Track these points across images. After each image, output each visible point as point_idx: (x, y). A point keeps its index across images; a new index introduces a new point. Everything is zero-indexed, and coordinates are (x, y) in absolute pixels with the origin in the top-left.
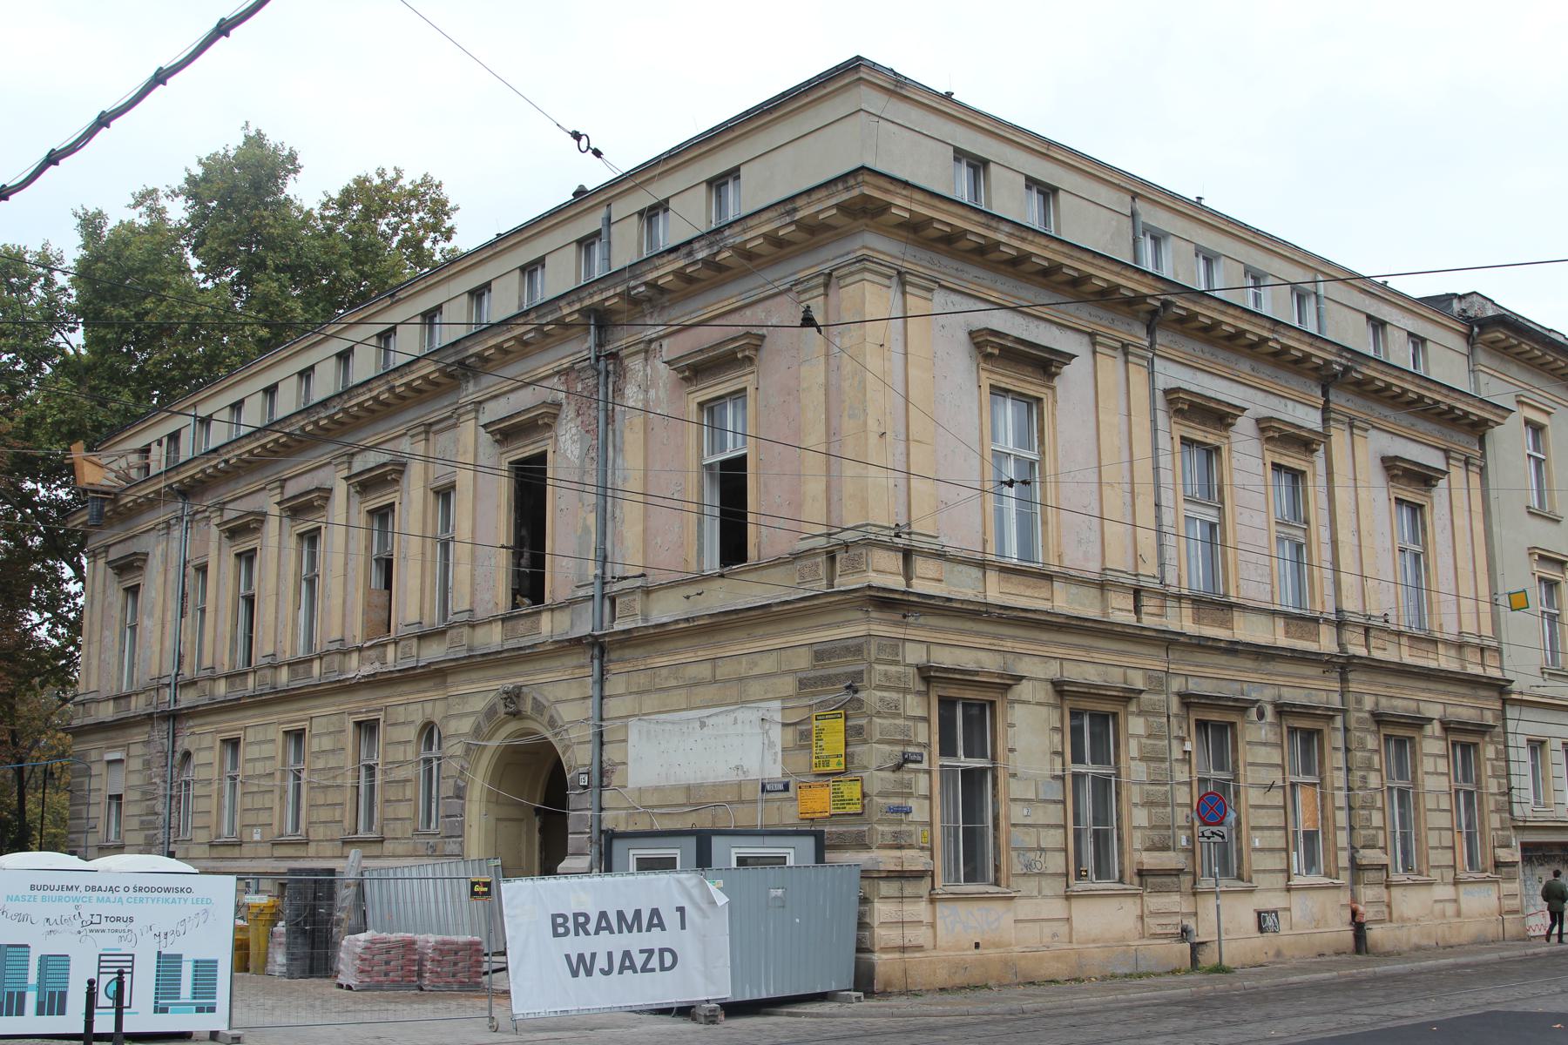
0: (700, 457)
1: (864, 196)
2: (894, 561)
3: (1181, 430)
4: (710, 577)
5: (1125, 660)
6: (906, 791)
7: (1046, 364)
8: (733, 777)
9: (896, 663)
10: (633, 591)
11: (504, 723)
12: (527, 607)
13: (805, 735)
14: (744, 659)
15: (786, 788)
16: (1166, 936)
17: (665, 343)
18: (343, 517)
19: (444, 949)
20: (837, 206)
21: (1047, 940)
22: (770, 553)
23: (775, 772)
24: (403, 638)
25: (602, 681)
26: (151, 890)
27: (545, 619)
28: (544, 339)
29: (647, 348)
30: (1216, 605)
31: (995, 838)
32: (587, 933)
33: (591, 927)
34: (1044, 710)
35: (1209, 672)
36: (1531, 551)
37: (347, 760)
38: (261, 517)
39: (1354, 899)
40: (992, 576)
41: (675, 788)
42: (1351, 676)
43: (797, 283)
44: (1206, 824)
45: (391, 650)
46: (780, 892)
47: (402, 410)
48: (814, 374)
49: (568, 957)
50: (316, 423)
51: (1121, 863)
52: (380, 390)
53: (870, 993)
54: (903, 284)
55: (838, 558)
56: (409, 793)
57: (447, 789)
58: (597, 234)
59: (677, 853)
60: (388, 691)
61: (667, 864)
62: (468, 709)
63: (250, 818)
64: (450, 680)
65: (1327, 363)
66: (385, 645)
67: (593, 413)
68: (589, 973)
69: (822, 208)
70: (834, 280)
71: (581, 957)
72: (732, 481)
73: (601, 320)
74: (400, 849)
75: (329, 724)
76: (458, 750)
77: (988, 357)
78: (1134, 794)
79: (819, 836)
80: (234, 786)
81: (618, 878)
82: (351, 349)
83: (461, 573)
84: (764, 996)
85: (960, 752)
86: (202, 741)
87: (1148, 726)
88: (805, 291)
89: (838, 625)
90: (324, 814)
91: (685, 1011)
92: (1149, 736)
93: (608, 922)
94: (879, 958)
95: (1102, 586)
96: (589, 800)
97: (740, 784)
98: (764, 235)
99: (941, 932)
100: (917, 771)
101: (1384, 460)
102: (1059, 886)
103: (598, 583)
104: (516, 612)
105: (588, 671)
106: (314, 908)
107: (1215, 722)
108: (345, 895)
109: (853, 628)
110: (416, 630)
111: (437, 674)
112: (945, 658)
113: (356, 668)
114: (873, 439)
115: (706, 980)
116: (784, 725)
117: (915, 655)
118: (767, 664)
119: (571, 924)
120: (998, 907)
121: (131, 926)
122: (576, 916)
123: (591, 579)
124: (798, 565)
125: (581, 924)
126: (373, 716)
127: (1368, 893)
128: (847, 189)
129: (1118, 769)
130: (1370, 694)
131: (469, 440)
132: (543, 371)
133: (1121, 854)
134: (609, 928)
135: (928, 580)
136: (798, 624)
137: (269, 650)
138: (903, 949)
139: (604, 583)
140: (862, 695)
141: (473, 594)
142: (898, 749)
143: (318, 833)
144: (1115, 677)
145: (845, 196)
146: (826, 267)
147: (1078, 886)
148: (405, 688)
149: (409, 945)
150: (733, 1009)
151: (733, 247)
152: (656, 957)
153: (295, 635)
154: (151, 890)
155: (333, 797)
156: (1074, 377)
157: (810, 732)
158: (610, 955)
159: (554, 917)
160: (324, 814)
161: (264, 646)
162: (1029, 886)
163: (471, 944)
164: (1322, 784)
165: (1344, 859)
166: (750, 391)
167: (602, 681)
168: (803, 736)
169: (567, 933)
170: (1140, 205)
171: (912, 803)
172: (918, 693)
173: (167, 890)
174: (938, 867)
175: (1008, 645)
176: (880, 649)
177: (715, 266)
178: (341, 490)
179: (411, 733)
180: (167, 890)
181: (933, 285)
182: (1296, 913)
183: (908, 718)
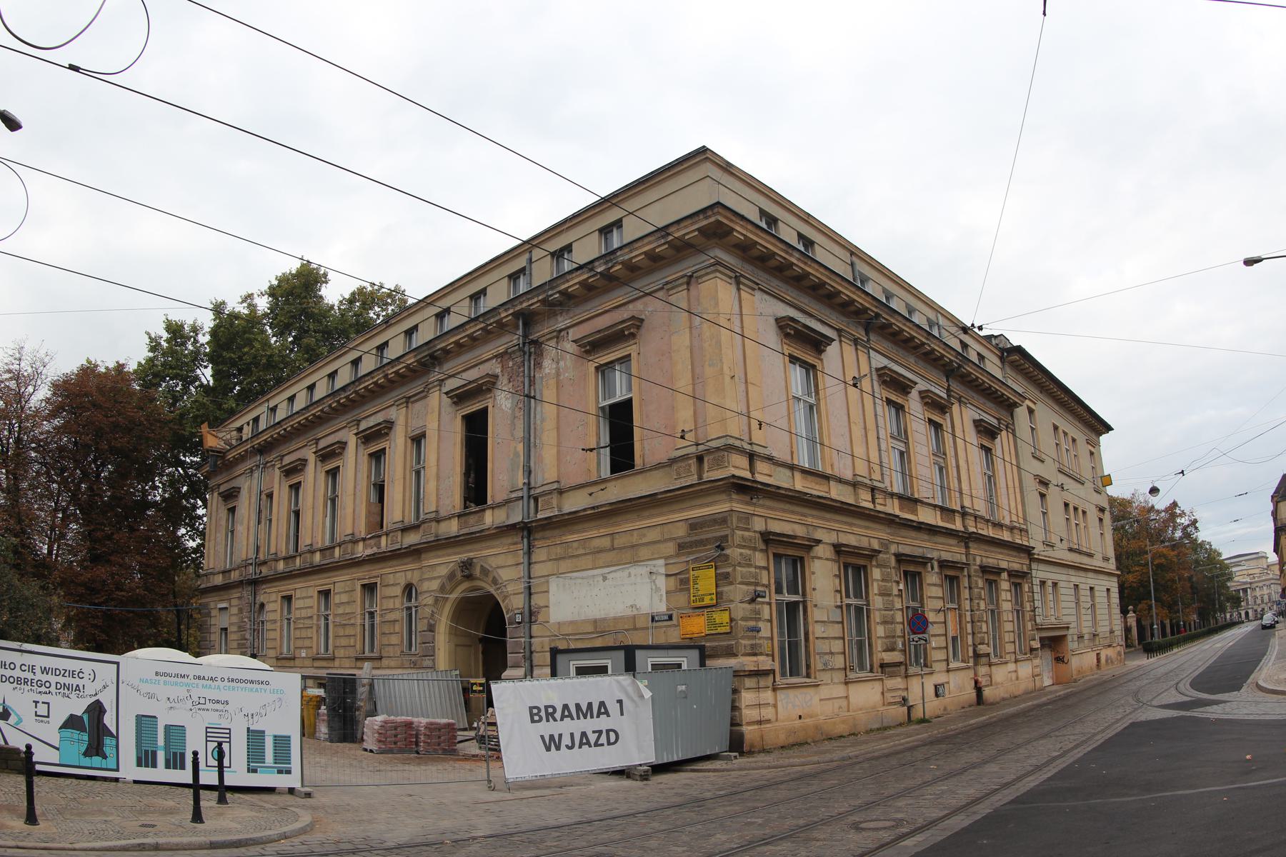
0: (597, 402)
1: (718, 222)
2: (743, 461)
3: (885, 394)
4: (605, 481)
5: (869, 533)
6: (757, 616)
7: (817, 344)
8: (629, 612)
9: (748, 530)
10: (551, 492)
11: (461, 582)
12: (473, 508)
13: (684, 582)
14: (635, 533)
15: (670, 618)
16: (895, 703)
17: (571, 331)
18: (354, 464)
19: (431, 727)
20: (698, 229)
21: (836, 711)
22: (652, 460)
23: (661, 607)
24: (392, 531)
25: (529, 553)
26: (240, 681)
27: (488, 514)
28: (487, 336)
29: (558, 335)
30: (910, 501)
31: (807, 647)
32: (555, 720)
33: (558, 715)
34: (829, 563)
35: (908, 541)
36: (1036, 476)
37: (357, 608)
38: (304, 462)
39: (976, 675)
40: (798, 475)
41: (585, 621)
42: (971, 544)
43: (667, 283)
44: (914, 633)
45: (384, 539)
46: (684, 687)
47: (392, 390)
48: (682, 340)
49: (542, 737)
50: (338, 402)
51: (871, 660)
52: (379, 378)
53: (742, 754)
54: (738, 283)
55: (706, 459)
56: (397, 629)
57: (422, 625)
58: (523, 270)
59: (609, 663)
60: (383, 565)
61: (602, 670)
62: (436, 574)
63: (299, 643)
64: (423, 556)
65: (951, 361)
66: (380, 536)
67: (521, 379)
68: (558, 748)
69: (689, 232)
70: (693, 280)
71: (552, 737)
72: (620, 419)
73: (528, 319)
74: (393, 664)
75: (345, 586)
76: (430, 601)
77: (787, 335)
78: (877, 617)
79: (702, 649)
80: (289, 624)
81: (560, 681)
82: (360, 358)
83: (430, 486)
84: (676, 759)
85: (785, 591)
86: (271, 597)
87: (882, 574)
88: (673, 288)
89: (707, 505)
90: (344, 642)
91: (621, 773)
92: (883, 580)
93: (569, 711)
94: (746, 729)
95: (855, 485)
96: (522, 631)
97: (634, 617)
98: (645, 253)
99: (780, 710)
100: (763, 603)
101: (974, 421)
102: (839, 676)
103: (525, 488)
104: (467, 511)
105: (520, 546)
106: (344, 699)
107: (911, 568)
108: (362, 691)
109: (720, 506)
110: (400, 525)
111: (415, 552)
112: (776, 527)
113: (361, 551)
114: (727, 379)
115: (638, 748)
116: (667, 575)
117: (759, 525)
118: (653, 535)
119: (543, 714)
120: (811, 691)
121: (227, 707)
122: (546, 707)
123: (521, 486)
124: (675, 467)
125: (550, 713)
126: (373, 581)
127: (983, 670)
128: (706, 218)
129: (868, 601)
130: (982, 556)
131: (437, 401)
132: (485, 356)
133: (871, 654)
134: (570, 716)
135: (765, 473)
136: (676, 507)
137: (308, 542)
138: (760, 722)
139: (530, 489)
140: (728, 552)
141: (438, 501)
142: (752, 588)
143: (340, 653)
144: (864, 543)
145: (705, 223)
146: (688, 272)
147: (852, 676)
148: (395, 562)
149: (409, 725)
150: (658, 769)
151: (622, 263)
152: (604, 735)
153: (324, 533)
154: (240, 681)
155: (349, 631)
156: (832, 350)
157: (688, 579)
158: (572, 735)
159: (531, 708)
160: (344, 642)
161: (305, 540)
162: (826, 677)
163: (449, 725)
164: (959, 609)
165: (971, 654)
166: (634, 355)
167: (529, 553)
168: (683, 583)
169: (540, 720)
170: (854, 259)
171: (761, 624)
172: (762, 550)
173: (252, 682)
174: (777, 666)
175: (810, 520)
176: (739, 519)
177: (611, 276)
178: (352, 441)
179: (398, 591)
180: (252, 682)
181: (756, 287)
182: (952, 685)
183: (756, 567)
